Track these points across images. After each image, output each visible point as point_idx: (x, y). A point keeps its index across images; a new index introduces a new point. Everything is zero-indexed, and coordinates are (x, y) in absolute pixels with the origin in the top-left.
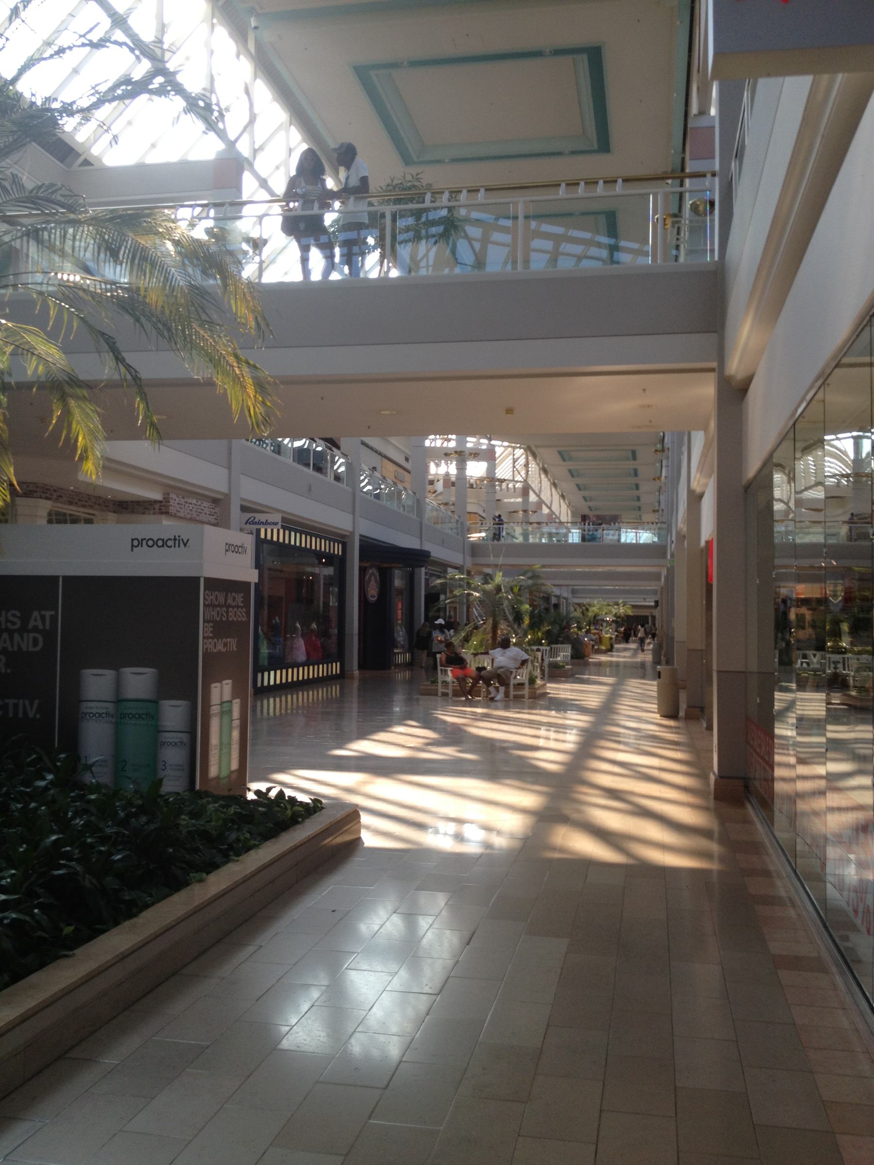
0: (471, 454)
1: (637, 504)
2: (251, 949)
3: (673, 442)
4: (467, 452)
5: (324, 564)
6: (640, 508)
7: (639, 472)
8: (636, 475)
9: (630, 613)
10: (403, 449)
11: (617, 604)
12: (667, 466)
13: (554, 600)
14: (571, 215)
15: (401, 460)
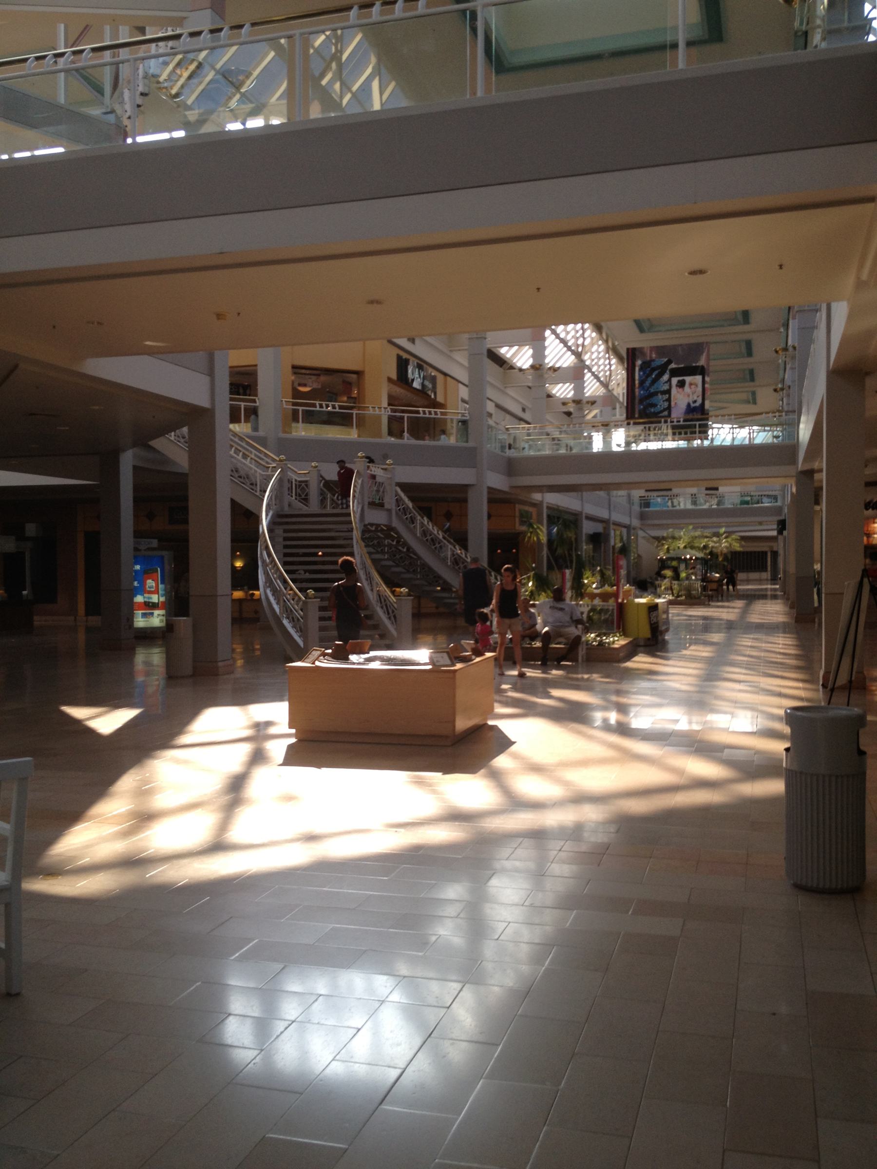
0: (588, 402)
1: (746, 363)
2: (658, 726)
3: (793, 381)
4: (585, 401)
5: (517, 550)
6: (752, 375)
7: (755, 349)
8: (750, 354)
9: (737, 547)
10: (521, 400)
11: (717, 535)
12: (792, 369)
13: (588, 528)
14: (726, 342)
15: (518, 411)
